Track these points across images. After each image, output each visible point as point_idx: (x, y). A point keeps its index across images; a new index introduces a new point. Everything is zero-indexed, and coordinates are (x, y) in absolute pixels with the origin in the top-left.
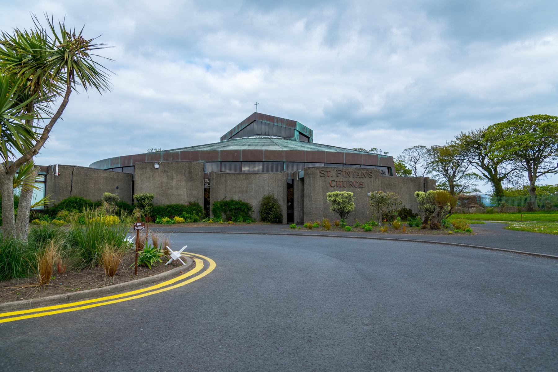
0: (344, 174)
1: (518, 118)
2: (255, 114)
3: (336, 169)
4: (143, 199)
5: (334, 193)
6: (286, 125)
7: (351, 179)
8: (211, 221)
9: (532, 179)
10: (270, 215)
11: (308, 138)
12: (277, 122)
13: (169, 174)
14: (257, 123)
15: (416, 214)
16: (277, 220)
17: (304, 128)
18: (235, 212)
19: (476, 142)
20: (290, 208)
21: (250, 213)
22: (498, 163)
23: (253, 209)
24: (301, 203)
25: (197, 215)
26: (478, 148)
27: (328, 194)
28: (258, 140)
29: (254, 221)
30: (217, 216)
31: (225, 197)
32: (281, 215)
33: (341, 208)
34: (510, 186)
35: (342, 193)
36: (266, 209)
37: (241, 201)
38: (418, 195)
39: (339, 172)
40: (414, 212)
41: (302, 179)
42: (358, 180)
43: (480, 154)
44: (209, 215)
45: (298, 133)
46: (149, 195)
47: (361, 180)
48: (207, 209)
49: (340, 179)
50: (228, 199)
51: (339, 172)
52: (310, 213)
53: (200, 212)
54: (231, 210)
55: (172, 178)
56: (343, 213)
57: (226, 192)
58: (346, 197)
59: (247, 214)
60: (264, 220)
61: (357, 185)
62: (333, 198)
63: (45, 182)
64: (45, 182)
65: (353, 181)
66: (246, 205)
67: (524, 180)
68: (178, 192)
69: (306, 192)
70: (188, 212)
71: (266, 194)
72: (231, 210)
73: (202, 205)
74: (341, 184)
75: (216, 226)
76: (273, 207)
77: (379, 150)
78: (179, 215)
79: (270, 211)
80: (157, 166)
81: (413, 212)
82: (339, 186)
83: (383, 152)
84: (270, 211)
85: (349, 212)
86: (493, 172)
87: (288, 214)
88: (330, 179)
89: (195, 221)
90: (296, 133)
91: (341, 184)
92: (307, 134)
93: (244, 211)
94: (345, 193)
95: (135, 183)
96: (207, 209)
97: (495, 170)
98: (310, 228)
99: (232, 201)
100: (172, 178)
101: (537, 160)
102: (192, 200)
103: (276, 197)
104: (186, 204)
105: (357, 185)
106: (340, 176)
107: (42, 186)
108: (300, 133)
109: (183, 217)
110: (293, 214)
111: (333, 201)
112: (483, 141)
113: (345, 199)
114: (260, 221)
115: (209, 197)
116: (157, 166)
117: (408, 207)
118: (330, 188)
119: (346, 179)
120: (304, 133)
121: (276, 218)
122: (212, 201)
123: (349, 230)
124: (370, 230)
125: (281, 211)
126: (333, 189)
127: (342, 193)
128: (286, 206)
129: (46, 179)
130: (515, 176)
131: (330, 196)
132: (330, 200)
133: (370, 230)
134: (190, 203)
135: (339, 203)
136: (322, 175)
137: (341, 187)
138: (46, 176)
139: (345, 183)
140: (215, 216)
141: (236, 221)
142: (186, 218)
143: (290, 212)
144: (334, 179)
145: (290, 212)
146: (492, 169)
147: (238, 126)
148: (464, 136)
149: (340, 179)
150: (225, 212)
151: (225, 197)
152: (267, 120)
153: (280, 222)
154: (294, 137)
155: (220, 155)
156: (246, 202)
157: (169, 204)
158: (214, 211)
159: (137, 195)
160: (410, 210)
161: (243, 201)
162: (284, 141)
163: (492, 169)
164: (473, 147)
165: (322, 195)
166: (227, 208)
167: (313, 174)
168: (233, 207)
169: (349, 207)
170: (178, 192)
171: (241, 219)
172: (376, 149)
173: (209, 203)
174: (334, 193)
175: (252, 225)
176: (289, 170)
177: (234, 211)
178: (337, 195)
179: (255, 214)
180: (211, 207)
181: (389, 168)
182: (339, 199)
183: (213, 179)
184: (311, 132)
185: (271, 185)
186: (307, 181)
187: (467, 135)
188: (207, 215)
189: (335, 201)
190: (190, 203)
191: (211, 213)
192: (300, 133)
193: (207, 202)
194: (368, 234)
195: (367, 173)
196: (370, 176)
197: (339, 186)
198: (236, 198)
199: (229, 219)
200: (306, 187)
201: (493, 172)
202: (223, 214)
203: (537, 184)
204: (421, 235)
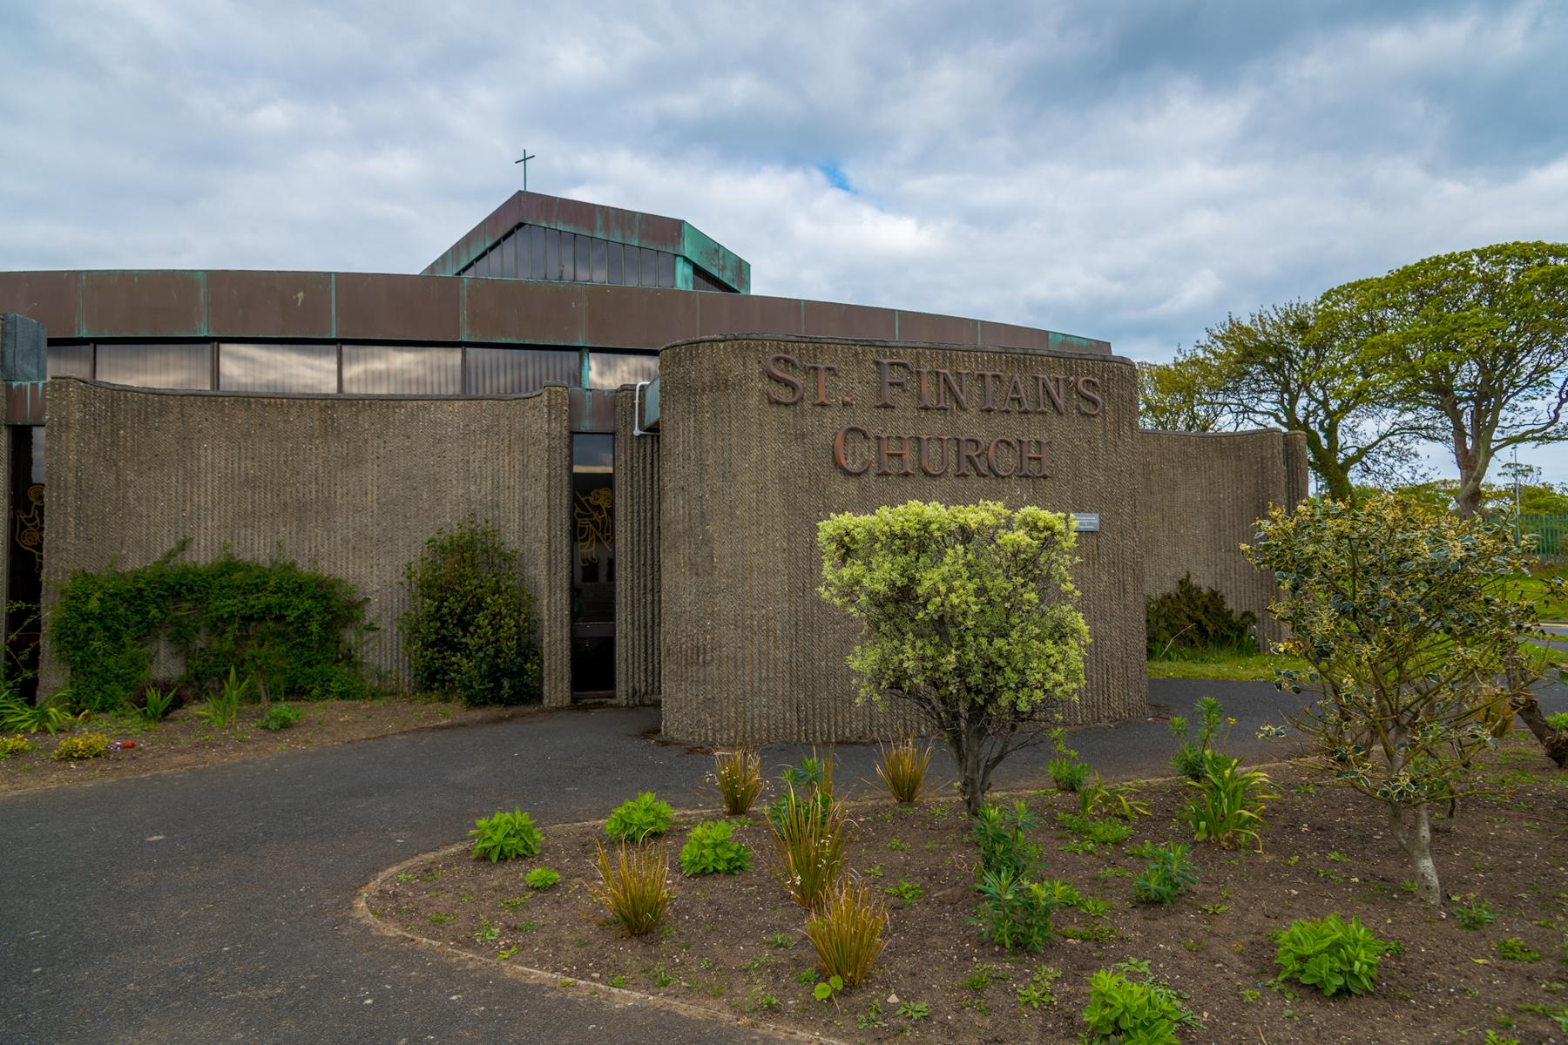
0: (928, 386)
1: (1438, 258)
3: (872, 354)
5: (887, 517)
6: (641, 239)
7: (970, 424)
9: (1471, 463)
12: (607, 227)
15: (1245, 614)
16: (508, 686)
17: (716, 250)
19: (1267, 348)
21: (350, 636)
22: (1345, 409)
23: (370, 615)
24: (650, 569)
26: (1278, 368)
27: (828, 527)
31: (183, 545)
32: (529, 649)
33: (961, 671)
34: (1370, 482)
35: (977, 515)
37: (496, 533)
39: (896, 375)
40: (1233, 605)
41: (654, 430)
42: (1015, 428)
43: (1286, 388)
45: (688, 270)
47: (1033, 431)
50: (202, 555)
51: (896, 375)
52: (696, 655)
60: (432, 681)
61: (1007, 461)
62: (882, 574)
65: (980, 434)
67: (1435, 462)
69: (674, 508)
71: (449, 520)
72: (217, 627)
74: (909, 455)
79: (464, 626)
81: (1230, 605)
82: (893, 466)
84: (464, 626)
86: (1324, 442)
88: (832, 423)
90: (683, 272)
91: (909, 455)
92: (726, 277)
97: (1331, 433)
99: (229, 566)
101: (1489, 396)
103: (511, 539)
106: (903, 401)
108: (698, 271)
110: (607, 645)
111: (878, 601)
112: (1295, 344)
117: (1203, 581)
119: (936, 425)
120: (715, 272)
122: (57, 569)
126: (852, 486)
127: (977, 515)
128: (562, 599)
130: (1387, 454)
131: (847, 549)
132: (849, 591)
136: (784, 394)
139: (934, 448)
144: (861, 419)
146: (1321, 434)
147: (456, 249)
148: (1236, 327)
149: (903, 422)
151: (183, 545)
152: (567, 222)
153: (527, 695)
155: (202, 295)
156: (325, 569)
158: (73, 641)
160: (1214, 594)
161: (304, 568)
163: (1321, 434)
164: (1263, 363)
167: (721, 384)
168: (225, 605)
174: (887, 517)
178: (919, 543)
179: (383, 648)
180: (50, 612)
183: (63, 425)
186: (677, 440)
187: (1246, 323)
189: (904, 595)
191: (46, 643)
192: (698, 271)
195: (1071, 387)
197: (893, 466)
198: (257, 548)
200: (675, 471)
201: (1324, 442)
203: (1495, 476)
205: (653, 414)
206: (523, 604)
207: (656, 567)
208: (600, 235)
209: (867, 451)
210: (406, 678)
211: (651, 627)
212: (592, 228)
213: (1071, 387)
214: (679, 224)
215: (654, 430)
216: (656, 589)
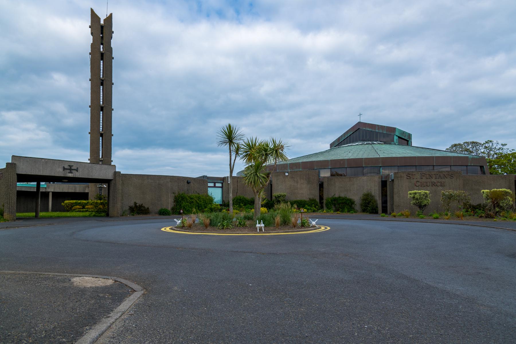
2: (359, 123)
4: (279, 197)
6: (387, 131)
7: (433, 180)
8: (325, 211)
10: (368, 207)
11: (408, 141)
12: (379, 129)
13: (295, 179)
14: (362, 133)
16: (374, 211)
17: (404, 133)
18: (342, 205)
20: (385, 202)
23: (356, 203)
24: (392, 198)
25: (315, 207)
28: (361, 147)
29: (356, 212)
30: (329, 208)
32: (377, 207)
35: (419, 191)
36: (365, 203)
38: (483, 192)
41: (393, 180)
42: (440, 180)
44: (323, 207)
45: (397, 138)
46: (282, 194)
47: (443, 180)
48: (321, 203)
49: (424, 180)
50: (337, 196)
53: (317, 205)
54: (339, 204)
55: (297, 182)
56: (421, 206)
57: (336, 190)
58: (424, 195)
59: (351, 206)
60: (364, 211)
62: (412, 196)
63: (222, 187)
64: (222, 187)
65: (435, 181)
66: (350, 200)
68: (271, 144)
69: (395, 190)
70: (309, 206)
71: (365, 192)
72: (339, 204)
73: (318, 200)
75: (328, 214)
76: (370, 202)
77: (495, 142)
78: (303, 207)
80: (287, 174)
83: (500, 143)
85: (425, 205)
87: (383, 207)
88: (415, 180)
89: (314, 211)
90: (396, 138)
93: (348, 205)
94: (422, 192)
95: (273, 186)
96: (321, 203)
98: (395, 216)
99: (340, 197)
100: (297, 182)
102: (311, 197)
103: (373, 194)
104: (307, 200)
105: (439, 184)
106: (424, 178)
107: (220, 189)
108: (399, 137)
109: (306, 208)
110: (387, 207)
113: (422, 196)
114: (361, 212)
115: (323, 195)
116: (287, 174)
118: (415, 187)
119: (429, 180)
120: (403, 137)
121: (373, 209)
122: (325, 197)
123: (422, 218)
124: (437, 218)
125: (377, 205)
126: (417, 188)
127: (419, 191)
128: (381, 201)
129: (222, 185)
131: (410, 194)
133: (437, 218)
134: (310, 199)
135: (417, 199)
137: (423, 186)
138: (222, 183)
140: (327, 208)
141: (342, 211)
142: (308, 209)
143: (384, 205)
145: (384, 205)
147: (344, 134)
150: (335, 205)
153: (376, 213)
154: (393, 141)
156: (350, 198)
157: (295, 200)
158: (327, 205)
159: (275, 194)
161: (348, 197)
162: (384, 146)
165: (407, 192)
166: (336, 202)
167: (401, 177)
168: (340, 201)
169: (425, 202)
170: (271, 144)
171: (346, 210)
172: (491, 141)
173: (323, 199)
175: (354, 214)
176: (385, 172)
177: (341, 205)
178: (415, 193)
179: (358, 207)
180: (325, 201)
181: (482, 167)
182: (417, 196)
184: (410, 136)
185: (370, 185)
186: (396, 182)
188: (322, 207)
189: (414, 197)
190: (310, 199)
191: (324, 205)
192: (399, 137)
193: (321, 198)
194: (438, 221)
195: (448, 175)
196: (451, 176)
198: (343, 195)
199: (337, 210)
202: (333, 206)
204: (481, 221)
205: (393, 178)
206: (376, 201)
207: (393, 197)
208: (377, 131)
209: (419, 184)
210: (359, 210)
211: (392, 205)
212: (375, 129)
213: (448, 175)
214: (395, 129)
215: (393, 180)
216: (393, 200)
